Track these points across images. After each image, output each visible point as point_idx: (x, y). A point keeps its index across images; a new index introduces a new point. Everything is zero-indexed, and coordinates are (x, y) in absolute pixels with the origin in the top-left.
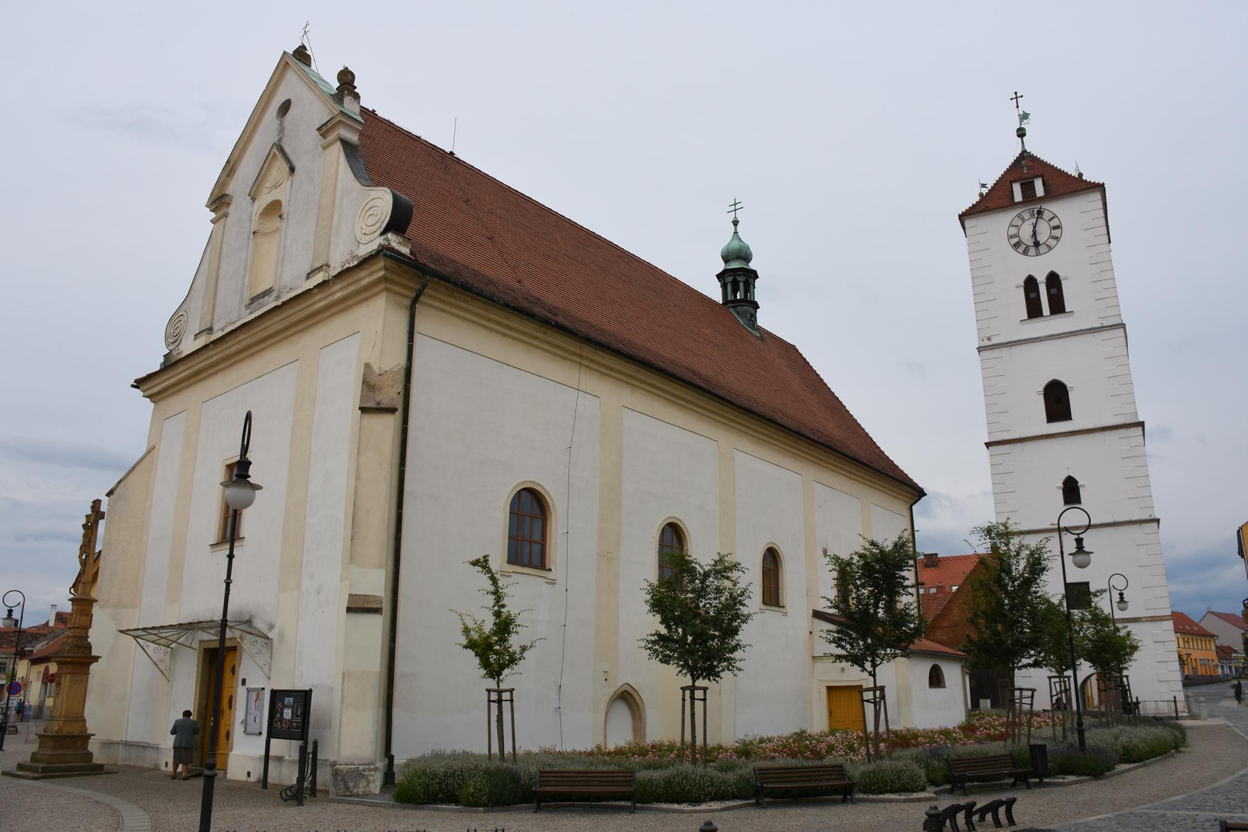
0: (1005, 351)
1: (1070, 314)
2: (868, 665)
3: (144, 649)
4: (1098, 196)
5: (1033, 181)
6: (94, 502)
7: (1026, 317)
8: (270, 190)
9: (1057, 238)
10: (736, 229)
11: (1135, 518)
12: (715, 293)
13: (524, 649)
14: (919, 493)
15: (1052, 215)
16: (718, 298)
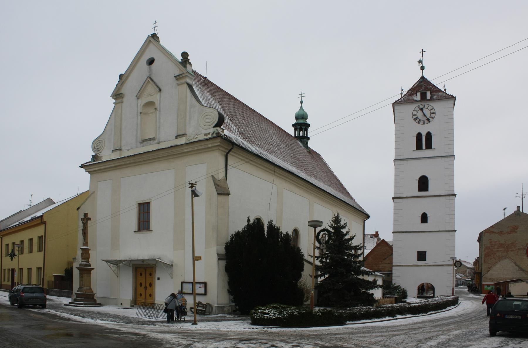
0: (405, 162)
1: (434, 150)
3: (110, 266)
4: (452, 102)
5: (426, 93)
7: (415, 149)
8: (147, 96)
9: (433, 118)
10: (301, 105)
11: (447, 230)
12: (291, 131)
13: (77, 262)
14: (368, 216)
15: (432, 108)
16: (293, 134)
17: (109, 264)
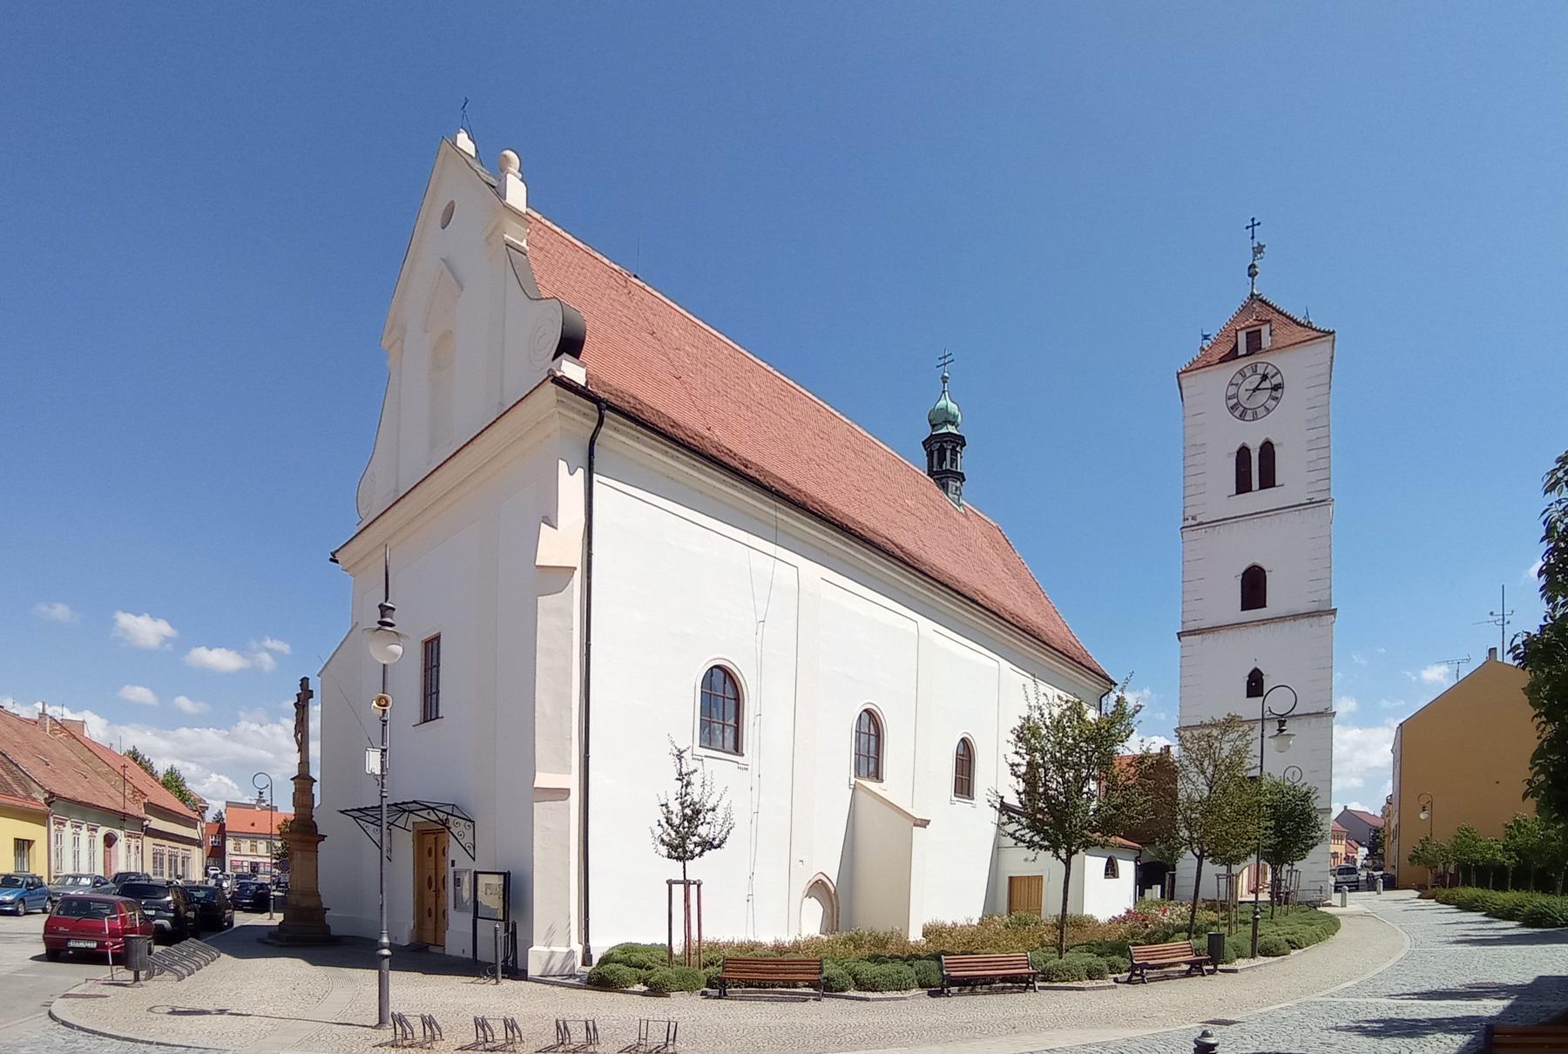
2: (1063, 853)
5: (1260, 331)
6: (302, 680)
7: (1234, 492)
9: (1275, 399)
17: (362, 823)
